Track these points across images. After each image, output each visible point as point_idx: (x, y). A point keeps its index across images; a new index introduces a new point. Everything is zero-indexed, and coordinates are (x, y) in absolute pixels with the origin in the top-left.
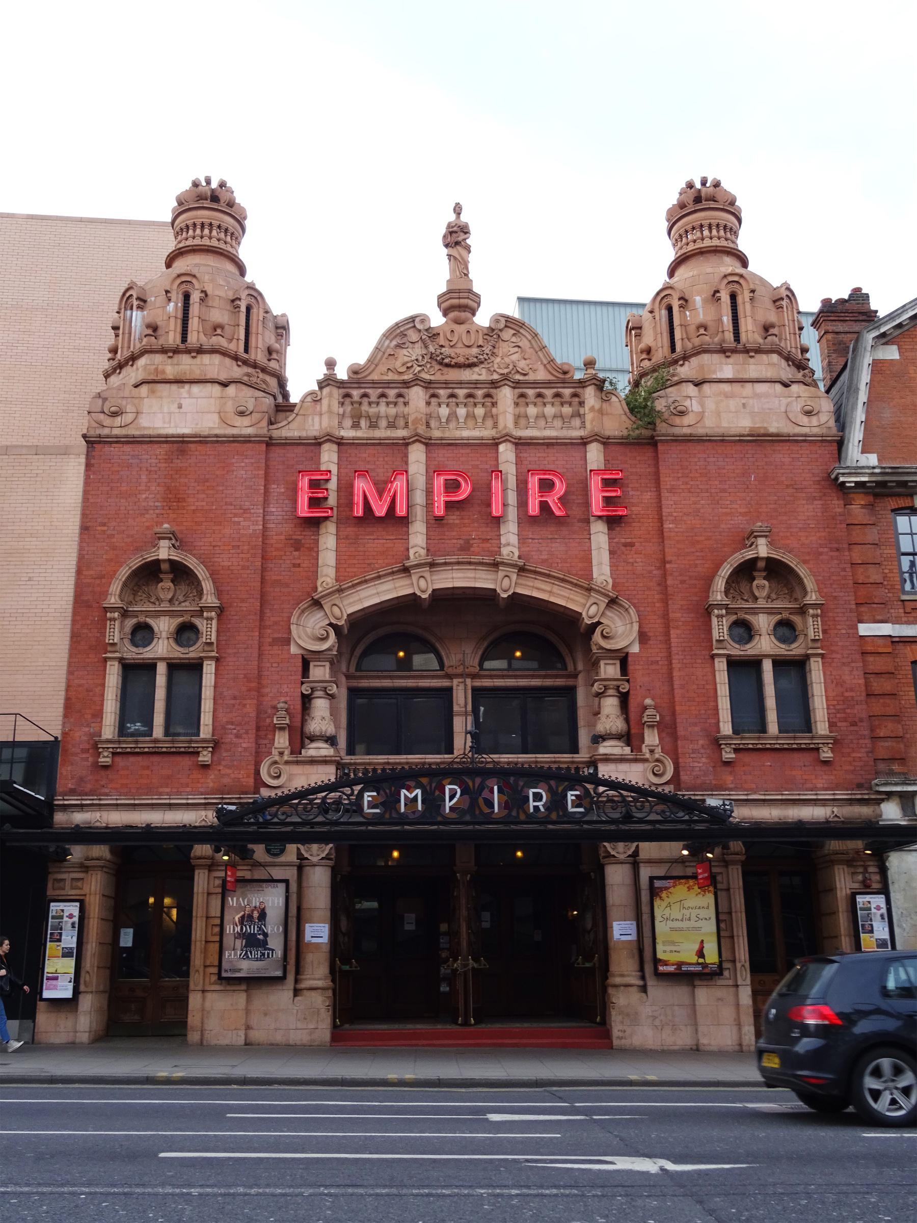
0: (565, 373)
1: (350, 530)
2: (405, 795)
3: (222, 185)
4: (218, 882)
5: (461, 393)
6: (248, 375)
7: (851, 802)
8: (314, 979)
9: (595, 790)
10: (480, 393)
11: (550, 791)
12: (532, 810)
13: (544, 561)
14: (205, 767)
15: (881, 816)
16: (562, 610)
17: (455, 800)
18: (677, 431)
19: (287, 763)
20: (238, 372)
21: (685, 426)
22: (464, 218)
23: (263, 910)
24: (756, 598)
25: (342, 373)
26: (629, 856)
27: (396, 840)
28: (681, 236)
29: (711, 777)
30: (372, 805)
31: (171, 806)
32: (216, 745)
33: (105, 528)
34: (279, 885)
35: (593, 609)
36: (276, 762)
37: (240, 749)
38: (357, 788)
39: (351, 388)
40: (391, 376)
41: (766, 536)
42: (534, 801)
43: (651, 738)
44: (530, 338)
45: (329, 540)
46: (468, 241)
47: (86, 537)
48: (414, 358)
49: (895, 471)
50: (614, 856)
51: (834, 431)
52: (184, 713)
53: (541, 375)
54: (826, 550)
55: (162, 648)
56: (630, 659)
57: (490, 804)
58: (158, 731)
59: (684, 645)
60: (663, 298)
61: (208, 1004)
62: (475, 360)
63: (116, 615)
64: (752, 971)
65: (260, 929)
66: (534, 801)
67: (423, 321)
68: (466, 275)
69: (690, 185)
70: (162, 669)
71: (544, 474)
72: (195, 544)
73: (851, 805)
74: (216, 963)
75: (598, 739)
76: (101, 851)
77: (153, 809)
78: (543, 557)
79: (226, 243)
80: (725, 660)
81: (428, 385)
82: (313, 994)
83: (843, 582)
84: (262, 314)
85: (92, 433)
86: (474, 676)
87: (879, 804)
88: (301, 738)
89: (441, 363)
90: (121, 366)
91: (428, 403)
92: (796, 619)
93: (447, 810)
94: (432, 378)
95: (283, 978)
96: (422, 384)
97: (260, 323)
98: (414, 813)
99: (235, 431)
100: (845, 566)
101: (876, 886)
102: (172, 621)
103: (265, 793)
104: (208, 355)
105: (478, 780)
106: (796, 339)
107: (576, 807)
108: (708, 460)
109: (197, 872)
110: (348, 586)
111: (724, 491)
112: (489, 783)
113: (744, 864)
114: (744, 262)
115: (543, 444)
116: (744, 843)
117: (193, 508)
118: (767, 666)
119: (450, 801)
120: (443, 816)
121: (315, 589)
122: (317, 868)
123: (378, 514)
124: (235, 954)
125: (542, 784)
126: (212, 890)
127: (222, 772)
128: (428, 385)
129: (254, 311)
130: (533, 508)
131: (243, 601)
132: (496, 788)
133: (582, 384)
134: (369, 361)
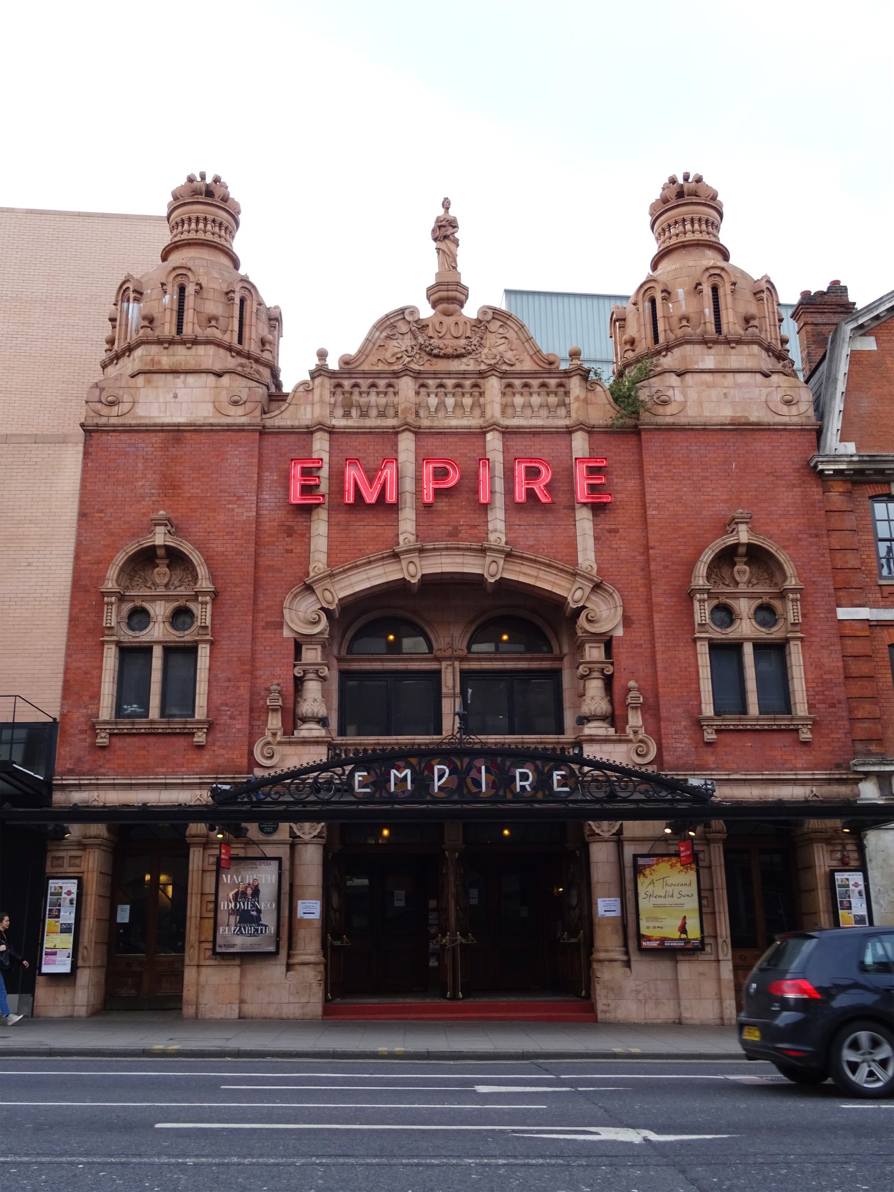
0: (551, 363)
1: (342, 517)
2: (395, 775)
3: (217, 180)
4: (213, 860)
5: (450, 383)
6: (242, 365)
7: (829, 782)
8: (307, 954)
9: (580, 770)
10: (468, 383)
11: (536, 771)
12: (518, 790)
13: (530, 547)
14: (200, 747)
15: (859, 795)
16: (548, 594)
17: (444, 780)
18: (660, 420)
19: (280, 743)
20: (232, 362)
21: (668, 415)
22: (452, 212)
23: (257, 887)
24: (737, 583)
25: (333, 364)
26: (614, 834)
27: (386, 819)
28: (664, 230)
29: (693, 758)
30: (362, 785)
31: (166, 786)
32: (210, 726)
33: (103, 515)
34: (272, 862)
35: (579, 594)
36: (269, 743)
37: (234, 730)
38: (348, 768)
39: (342, 379)
40: (381, 367)
41: (747, 523)
42: (521, 781)
43: (635, 719)
44: (516, 329)
45: (320, 526)
46: (456, 235)
47: (83, 523)
48: (403, 349)
49: (873, 459)
50: (598, 834)
51: (813, 420)
52: (179, 695)
53: (528, 365)
54: (805, 536)
55: (158, 631)
56: (614, 642)
57: (478, 784)
58: (154, 713)
59: (666, 628)
60: (646, 291)
61: (202, 979)
62: (463, 351)
63: (113, 599)
64: (733, 946)
65: (254, 905)
66: (521, 781)
67: (412, 313)
68: (455, 268)
69: (673, 181)
70: (157, 652)
71: (531, 462)
72: (190, 530)
73: (829, 784)
74: (211, 939)
75: (583, 720)
76: (98, 829)
77: (149, 789)
78: (529, 543)
79: (220, 236)
80: (706, 643)
81: (417, 375)
82: (305, 969)
83: (822, 567)
84: (255, 306)
85: (89, 422)
86: (462, 659)
87: (857, 784)
88: (293, 719)
89: (430, 354)
90: (118, 357)
91: (418, 393)
92: (777, 603)
93: (436, 790)
94: (421, 368)
95: (276, 953)
96: (412, 374)
97: (254, 315)
98: (403, 792)
99: (229, 420)
100: (824, 551)
101: (854, 863)
102: (167, 605)
103: (258, 773)
104: (203, 346)
105: (466, 761)
106: (776, 330)
107: (562, 786)
108: (690, 448)
109: (192, 850)
110: (339, 571)
111: (706, 478)
112: (477, 763)
113: (725, 842)
115: (529, 433)
116: (725, 822)
117: (188, 495)
118: (748, 649)
119: (439, 780)
120: (432, 796)
121: (307, 574)
122: (309, 846)
123: (368, 501)
124: (229, 930)
125: (528, 764)
126: (207, 868)
127: (217, 753)
128: (417, 375)
129: (248, 303)
130: (520, 495)
131: (237, 585)
132: (483, 768)
133: (567, 374)
134: (359, 351)
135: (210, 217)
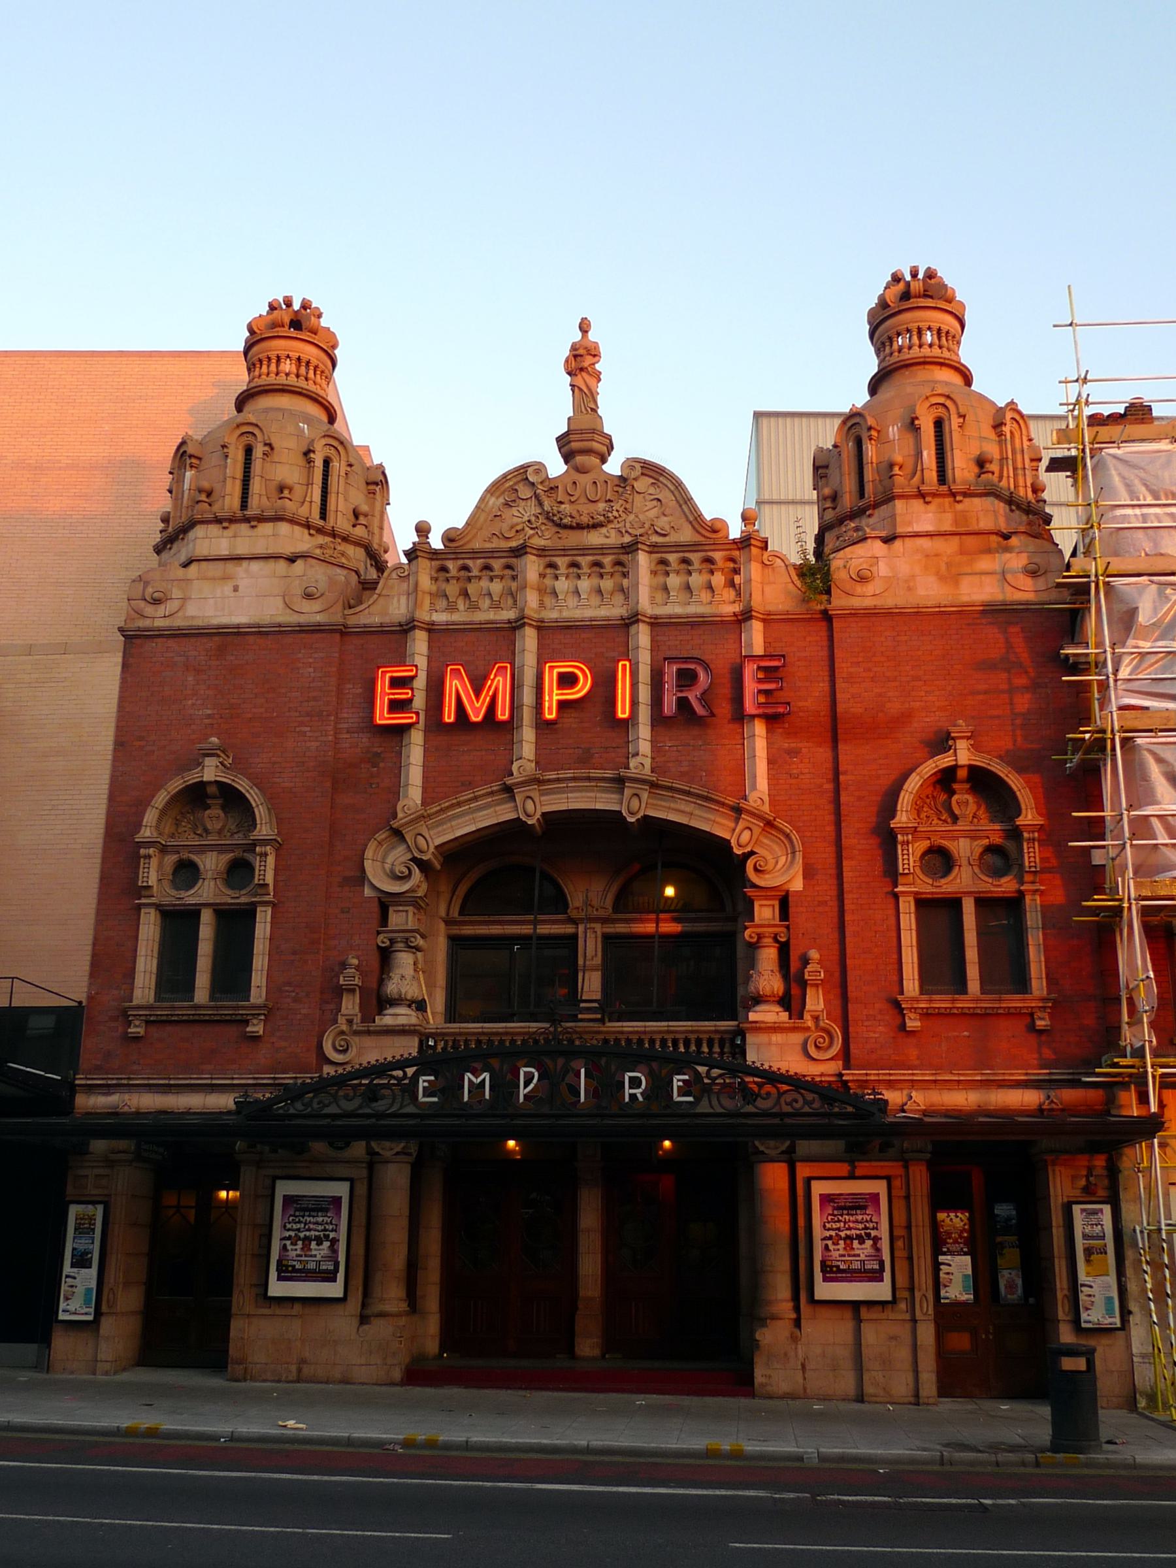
3: (305, 305)
6: (321, 547)
11: (650, 1075)
12: (627, 1100)
13: (683, 774)
14: (255, 1039)
17: (532, 1086)
19: (356, 1033)
20: (301, 541)
21: (865, 597)
22: (592, 336)
24: (955, 819)
26: (783, 1152)
28: (883, 344)
30: (427, 1093)
32: (268, 1012)
36: (343, 1033)
37: (299, 1017)
38: (410, 1071)
40: (496, 544)
41: (968, 738)
42: (630, 1088)
43: (815, 1002)
44: (673, 488)
46: (598, 367)
48: (526, 518)
50: (763, 1153)
52: (232, 970)
53: (686, 535)
55: (208, 891)
58: (201, 995)
62: (602, 518)
63: (151, 851)
66: (630, 1088)
67: (538, 471)
68: (594, 410)
69: (896, 278)
77: (193, 1091)
78: (682, 769)
80: (911, 899)
81: (542, 552)
84: (344, 468)
86: (605, 921)
88: (378, 1001)
89: (559, 525)
91: (542, 576)
92: (1010, 846)
93: (521, 1099)
96: (535, 552)
98: (480, 1102)
99: (302, 619)
101: (1102, 1193)
103: (328, 1070)
104: (271, 524)
105: (561, 1061)
108: (899, 638)
111: (918, 678)
112: (574, 1064)
114: (968, 379)
115: (686, 624)
117: (250, 716)
118: (968, 907)
121: (395, 816)
122: (390, 1165)
123: (474, 719)
125: (641, 1067)
128: (542, 552)
129: (335, 464)
130: (669, 705)
132: (583, 1071)
134: (468, 524)
135: (314, 362)
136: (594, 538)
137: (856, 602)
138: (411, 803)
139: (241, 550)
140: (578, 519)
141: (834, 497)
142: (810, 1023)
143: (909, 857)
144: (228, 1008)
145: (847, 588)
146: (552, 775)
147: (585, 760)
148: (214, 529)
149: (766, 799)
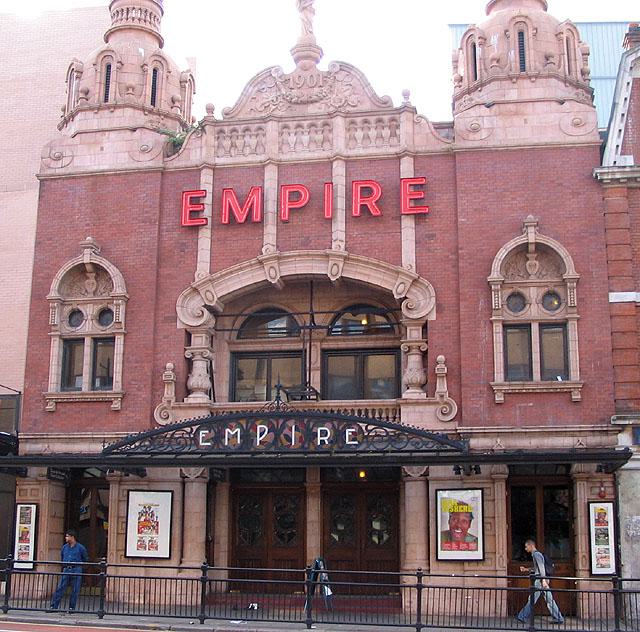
0: (385, 103)
1: (222, 234)
6: (151, 121)
9: (366, 427)
20: (141, 119)
25: (218, 116)
27: (364, 463)
35: (401, 287)
36: (165, 408)
38: (195, 428)
43: (442, 387)
45: (205, 239)
53: (367, 106)
55: (88, 328)
67: (277, 71)
70: (88, 342)
76: (503, 468)
91: (281, 134)
92: (559, 290)
99: (139, 165)
110: (215, 274)
113: (507, 482)
116: (509, 466)
123: (239, 221)
128: (280, 119)
129: (160, 72)
133: (399, 111)
135: (150, 11)
136: (312, 109)
137: (470, 144)
138: (203, 272)
139: (106, 126)
140: (303, 99)
141: (461, 79)
142: (438, 399)
143: (498, 300)
144: (101, 394)
145: (465, 136)
146: (287, 254)
147: (306, 245)
148: (90, 114)
149: (414, 265)
